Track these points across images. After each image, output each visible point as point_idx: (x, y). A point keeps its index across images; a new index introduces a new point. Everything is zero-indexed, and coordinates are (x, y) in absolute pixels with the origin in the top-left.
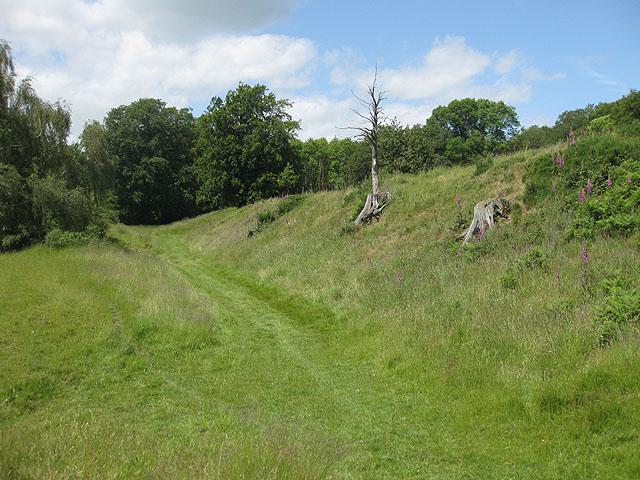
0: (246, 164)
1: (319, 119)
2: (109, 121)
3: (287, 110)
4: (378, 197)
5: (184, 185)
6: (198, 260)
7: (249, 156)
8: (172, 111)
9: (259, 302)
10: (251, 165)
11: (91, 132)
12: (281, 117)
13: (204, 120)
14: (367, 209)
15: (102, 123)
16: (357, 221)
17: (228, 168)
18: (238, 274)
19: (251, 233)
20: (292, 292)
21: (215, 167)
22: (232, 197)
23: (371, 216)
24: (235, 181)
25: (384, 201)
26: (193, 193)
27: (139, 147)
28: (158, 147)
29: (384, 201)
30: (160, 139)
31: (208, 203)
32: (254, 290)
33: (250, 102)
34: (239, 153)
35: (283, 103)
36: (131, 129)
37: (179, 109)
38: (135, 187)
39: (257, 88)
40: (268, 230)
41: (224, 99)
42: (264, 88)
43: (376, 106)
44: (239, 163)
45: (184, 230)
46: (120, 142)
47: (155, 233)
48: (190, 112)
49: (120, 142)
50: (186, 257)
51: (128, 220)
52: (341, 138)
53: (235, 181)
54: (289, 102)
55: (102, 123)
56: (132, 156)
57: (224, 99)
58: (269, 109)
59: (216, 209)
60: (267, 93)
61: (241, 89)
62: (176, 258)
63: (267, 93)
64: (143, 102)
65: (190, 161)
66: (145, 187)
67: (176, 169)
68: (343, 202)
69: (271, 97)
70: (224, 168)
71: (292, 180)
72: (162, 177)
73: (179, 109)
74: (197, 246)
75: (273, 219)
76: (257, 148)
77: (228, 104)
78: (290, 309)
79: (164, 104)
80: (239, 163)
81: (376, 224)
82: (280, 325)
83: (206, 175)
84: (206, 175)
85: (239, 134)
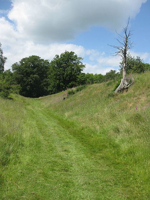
0: (66, 77)
1: (89, 69)
2: (21, 62)
3: (81, 60)
4: (127, 80)
5: (45, 85)
6: (42, 108)
7: (67, 75)
8: (42, 60)
9: (62, 129)
10: (67, 79)
11: (15, 66)
12: (79, 63)
13: (52, 62)
14: (121, 86)
15: (19, 63)
16: (116, 91)
17: (59, 79)
18: (56, 114)
19: (64, 98)
20: (83, 125)
21: (55, 78)
22: (59, 89)
23: (124, 89)
24: (62, 84)
25: (130, 82)
26: (47, 88)
27: (30, 71)
28: (37, 71)
29: (130, 82)
30: (37, 69)
31: (52, 91)
32: (61, 122)
33: (68, 57)
34: (64, 74)
35: (80, 58)
36: (28, 65)
37: (45, 60)
38: (28, 84)
39: (71, 52)
40: (72, 97)
41: (60, 55)
42: (74, 53)
43: (127, 38)
44: (63, 77)
45: (42, 99)
46: (24, 69)
47: (28, 100)
48: (48, 61)
49: (24, 69)
50: (38, 107)
51: (21, 93)
52: (98, 73)
53: (62, 84)
54: (82, 58)
55: (19, 63)
56: (28, 74)
57: (60, 55)
58: (75, 60)
59: (54, 93)
60: (74, 55)
61: (66, 53)
62: (34, 107)
63: (74, 55)
64: (33, 56)
65: (46, 77)
66: (31, 85)
67: (42, 80)
68: (106, 85)
69: (76, 56)
70: (58, 79)
71: (82, 79)
72: (36, 81)
73: (45, 60)
74: (43, 104)
75: (74, 93)
76: (70, 73)
77: (61, 58)
78: (81, 136)
79: (40, 58)
80: (63, 77)
81: (125, 94)
82: (75, 153)
83: (52, 82)
84: (52, 82)
85: (64, 68)
